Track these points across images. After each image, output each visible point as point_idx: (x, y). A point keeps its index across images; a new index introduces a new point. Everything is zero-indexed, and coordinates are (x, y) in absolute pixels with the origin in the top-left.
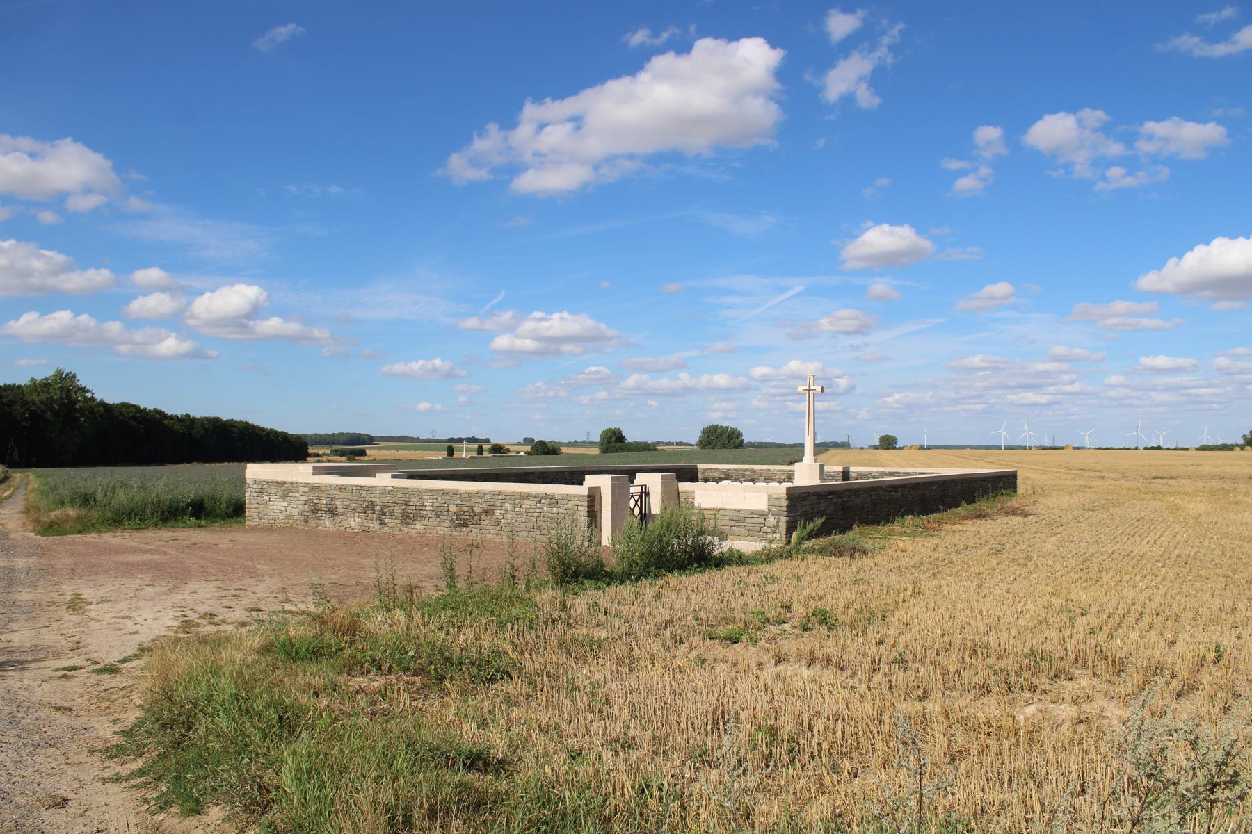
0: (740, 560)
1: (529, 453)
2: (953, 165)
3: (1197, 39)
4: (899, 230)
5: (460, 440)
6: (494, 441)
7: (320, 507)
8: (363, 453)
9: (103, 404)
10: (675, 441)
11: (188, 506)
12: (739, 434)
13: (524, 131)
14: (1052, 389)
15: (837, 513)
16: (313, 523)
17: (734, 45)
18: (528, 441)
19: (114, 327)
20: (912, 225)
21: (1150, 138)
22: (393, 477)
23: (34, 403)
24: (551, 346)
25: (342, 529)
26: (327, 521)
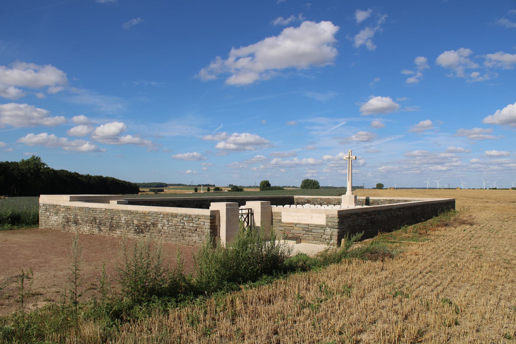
0: (304, 265)
1: (229, 191)
2: (407, 72)
3: (507, 20)
4: (384, 99)
5: (200, 186)
6: (216, 186)
7: (71, 219)
8: (162, 191)
9: (53, 170)
10: (291, 186)
11: (8, 218)
12: (318, 183)
13: (231, 60)
14: (448, 164)
15: (370, 225)
16: (67, 229)
17: (318, 25)
19: (64, 140)
20: (390, 97)
21: (490, 61)
22: (119, 203)
23: (22, 170)
24: (241, 147)
25: (81, 233)
26: (73, 228)
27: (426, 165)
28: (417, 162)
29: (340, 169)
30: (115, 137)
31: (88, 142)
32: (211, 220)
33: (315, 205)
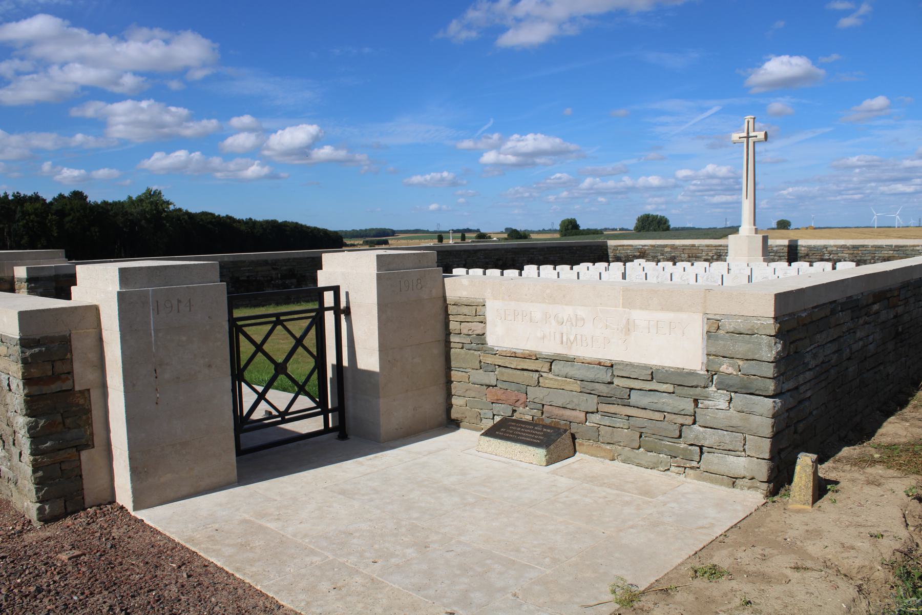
9: (187, 213)
19: (216, 161)
23: (131, 214)
24: (529, 159)
27: (873, 184)
28: (855, 179)
29: (709, 195)
30: (303, 152)
31: (257, 162)
32: (25, 361)
33: (659, 261)
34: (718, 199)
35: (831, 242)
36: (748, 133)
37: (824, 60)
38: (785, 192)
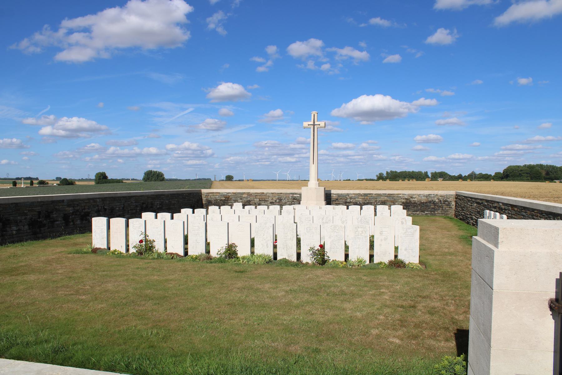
1: (59, 185)
5: (20, 179)
6: (40, 179)
13: (62, 32)
14: (297, 156)
18: (58, 179)
27: (275, 156)
34: (191, 162)
35: (352, 192)
36: (314, 122)
37: (250, 87)
38: (229, 159)
